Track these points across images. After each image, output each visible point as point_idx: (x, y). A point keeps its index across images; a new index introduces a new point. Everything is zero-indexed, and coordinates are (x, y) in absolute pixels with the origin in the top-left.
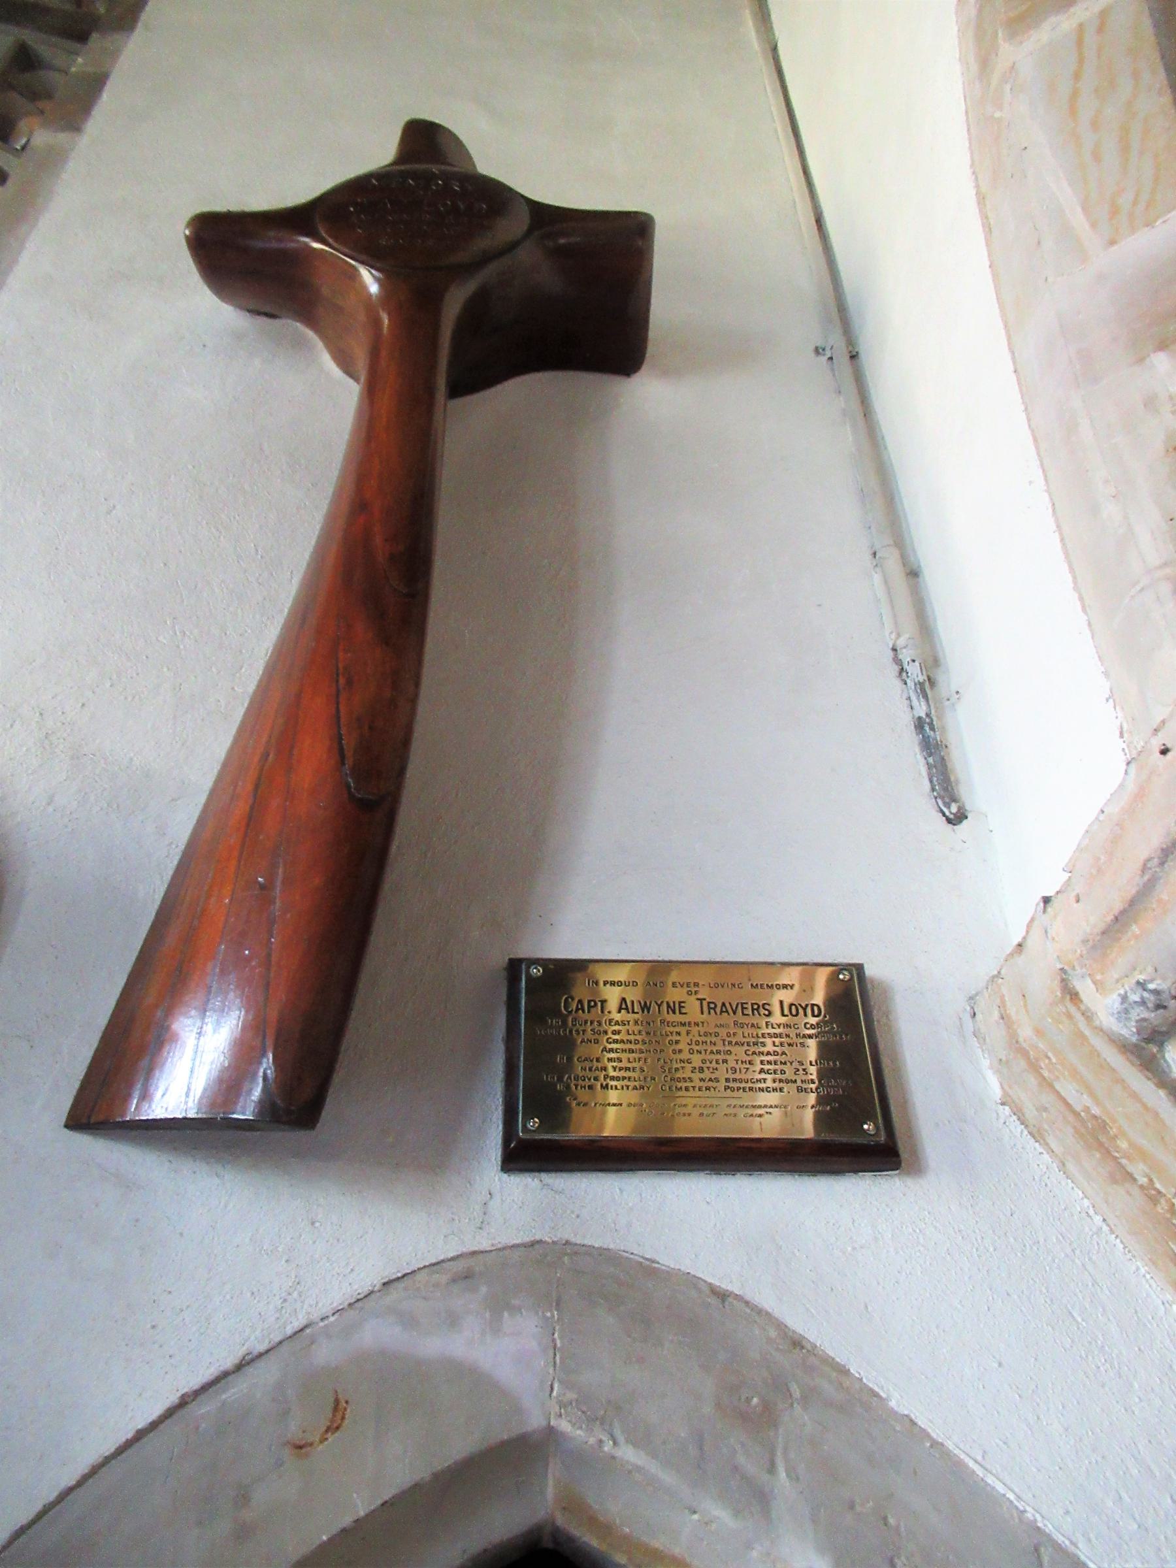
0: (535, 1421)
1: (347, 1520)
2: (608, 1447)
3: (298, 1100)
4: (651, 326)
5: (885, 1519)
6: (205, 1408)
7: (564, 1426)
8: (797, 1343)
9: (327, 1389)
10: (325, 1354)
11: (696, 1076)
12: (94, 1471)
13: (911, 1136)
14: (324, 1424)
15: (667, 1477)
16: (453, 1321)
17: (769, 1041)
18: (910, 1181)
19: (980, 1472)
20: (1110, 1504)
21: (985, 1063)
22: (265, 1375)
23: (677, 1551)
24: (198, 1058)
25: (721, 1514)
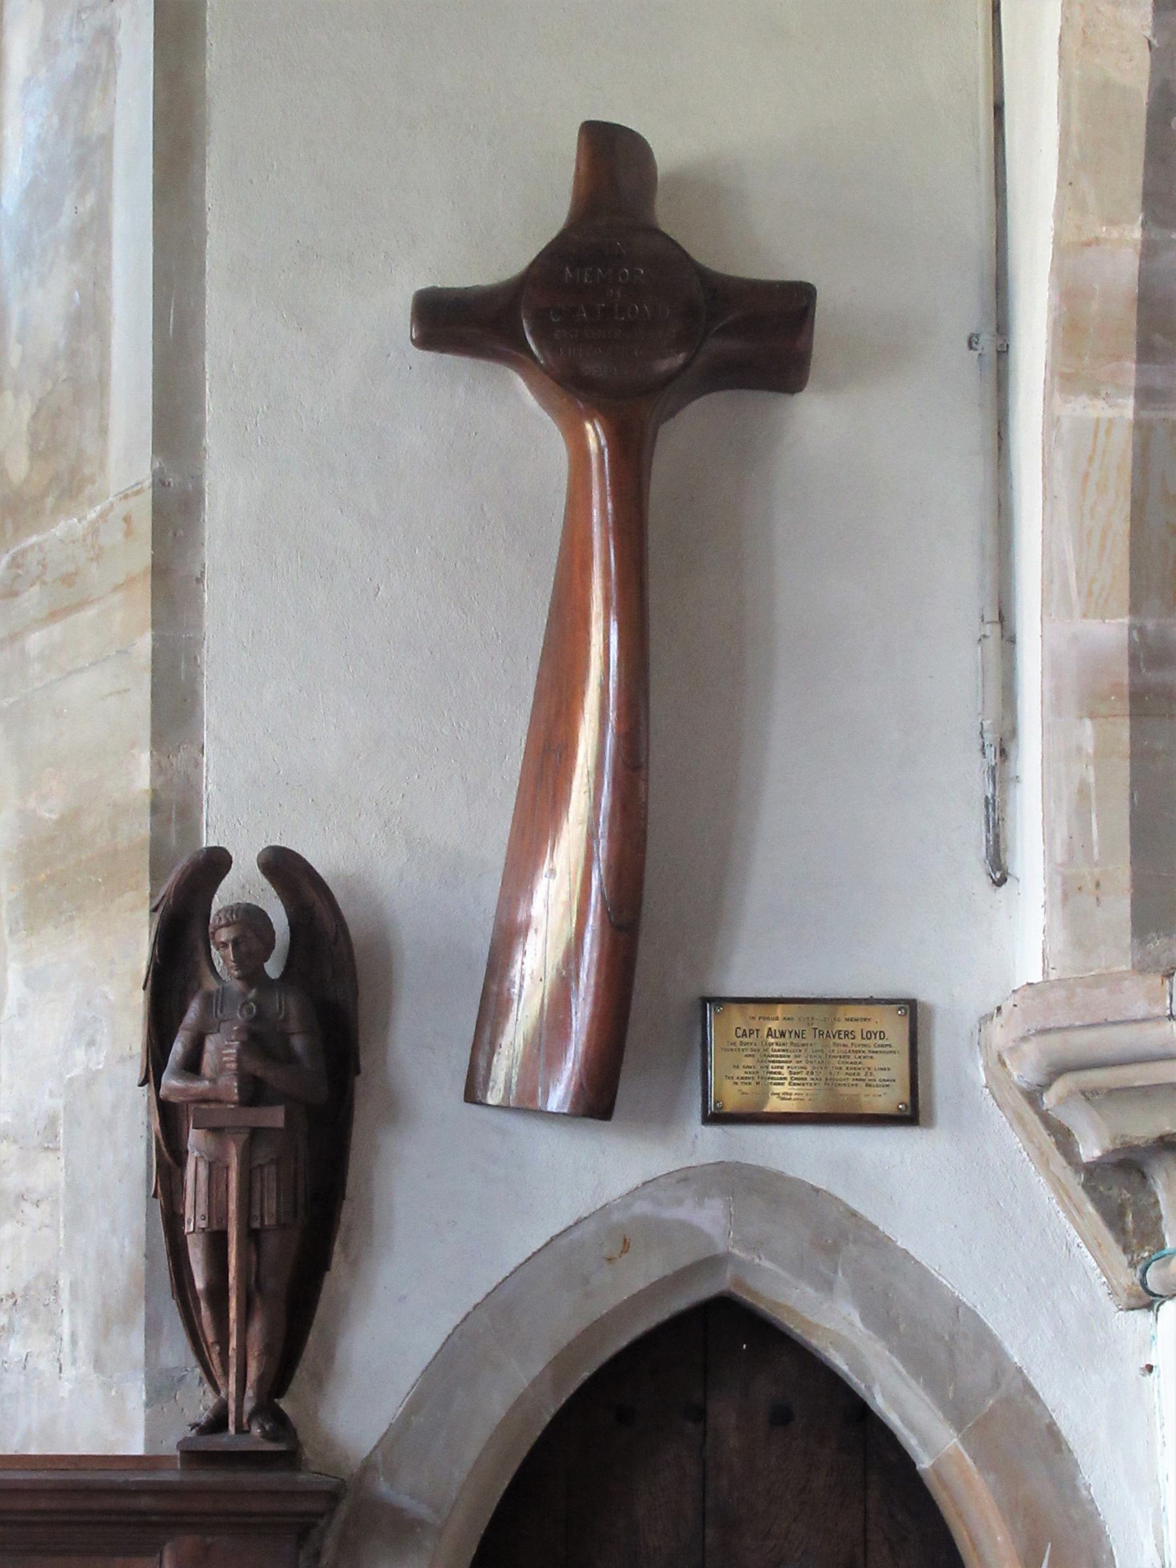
0: (721, 1248)
1: (635, 1291)
2: (757, 1260)
3: (598, 1101)
4: (818, 301)
5: (887, 1294)
6: (563, 1242)
7: (736, 1251)
8: (854, 1214)
9: (615, 1234)
10: (616, 1217)
11: (808, 1077)
12: (516, 1269)
13: (930, 1102)
14: (621, 1248)
15: (783, 1273)
16: (679, 1202)
17: (852, 1055)
18: (925, 1131)
19: (936, 1275)
20: (996, 1290)
21: (981, 1062)
22: (590, 1227)
23: (790, 1304)
24: (558, 1097)
25: (810, 1291)
